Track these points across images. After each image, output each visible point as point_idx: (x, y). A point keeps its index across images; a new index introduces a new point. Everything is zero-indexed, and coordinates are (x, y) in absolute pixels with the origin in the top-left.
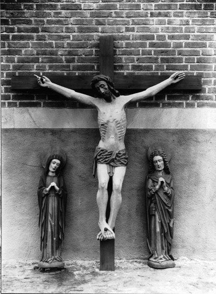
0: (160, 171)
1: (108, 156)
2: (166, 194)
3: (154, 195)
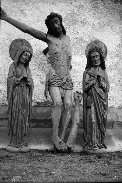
3: (91, 88)
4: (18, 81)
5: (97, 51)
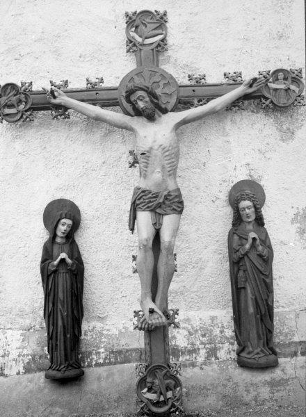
0: (249, 222)
1: (152, 200)
2: (260, 256)
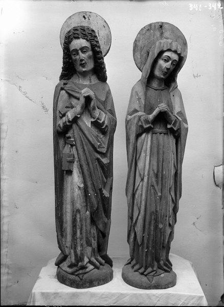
4: (147, 121)
5: (85, 37)
